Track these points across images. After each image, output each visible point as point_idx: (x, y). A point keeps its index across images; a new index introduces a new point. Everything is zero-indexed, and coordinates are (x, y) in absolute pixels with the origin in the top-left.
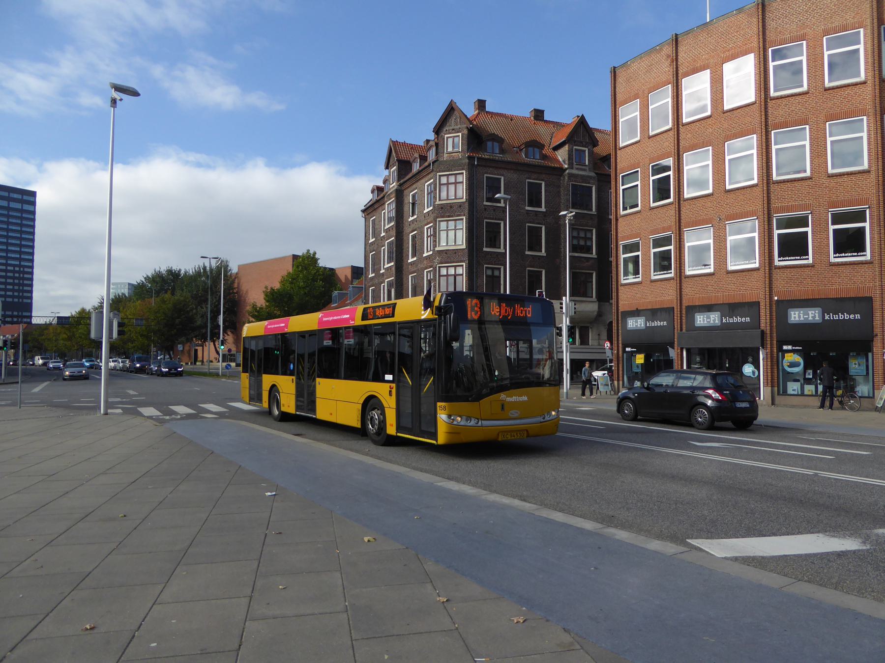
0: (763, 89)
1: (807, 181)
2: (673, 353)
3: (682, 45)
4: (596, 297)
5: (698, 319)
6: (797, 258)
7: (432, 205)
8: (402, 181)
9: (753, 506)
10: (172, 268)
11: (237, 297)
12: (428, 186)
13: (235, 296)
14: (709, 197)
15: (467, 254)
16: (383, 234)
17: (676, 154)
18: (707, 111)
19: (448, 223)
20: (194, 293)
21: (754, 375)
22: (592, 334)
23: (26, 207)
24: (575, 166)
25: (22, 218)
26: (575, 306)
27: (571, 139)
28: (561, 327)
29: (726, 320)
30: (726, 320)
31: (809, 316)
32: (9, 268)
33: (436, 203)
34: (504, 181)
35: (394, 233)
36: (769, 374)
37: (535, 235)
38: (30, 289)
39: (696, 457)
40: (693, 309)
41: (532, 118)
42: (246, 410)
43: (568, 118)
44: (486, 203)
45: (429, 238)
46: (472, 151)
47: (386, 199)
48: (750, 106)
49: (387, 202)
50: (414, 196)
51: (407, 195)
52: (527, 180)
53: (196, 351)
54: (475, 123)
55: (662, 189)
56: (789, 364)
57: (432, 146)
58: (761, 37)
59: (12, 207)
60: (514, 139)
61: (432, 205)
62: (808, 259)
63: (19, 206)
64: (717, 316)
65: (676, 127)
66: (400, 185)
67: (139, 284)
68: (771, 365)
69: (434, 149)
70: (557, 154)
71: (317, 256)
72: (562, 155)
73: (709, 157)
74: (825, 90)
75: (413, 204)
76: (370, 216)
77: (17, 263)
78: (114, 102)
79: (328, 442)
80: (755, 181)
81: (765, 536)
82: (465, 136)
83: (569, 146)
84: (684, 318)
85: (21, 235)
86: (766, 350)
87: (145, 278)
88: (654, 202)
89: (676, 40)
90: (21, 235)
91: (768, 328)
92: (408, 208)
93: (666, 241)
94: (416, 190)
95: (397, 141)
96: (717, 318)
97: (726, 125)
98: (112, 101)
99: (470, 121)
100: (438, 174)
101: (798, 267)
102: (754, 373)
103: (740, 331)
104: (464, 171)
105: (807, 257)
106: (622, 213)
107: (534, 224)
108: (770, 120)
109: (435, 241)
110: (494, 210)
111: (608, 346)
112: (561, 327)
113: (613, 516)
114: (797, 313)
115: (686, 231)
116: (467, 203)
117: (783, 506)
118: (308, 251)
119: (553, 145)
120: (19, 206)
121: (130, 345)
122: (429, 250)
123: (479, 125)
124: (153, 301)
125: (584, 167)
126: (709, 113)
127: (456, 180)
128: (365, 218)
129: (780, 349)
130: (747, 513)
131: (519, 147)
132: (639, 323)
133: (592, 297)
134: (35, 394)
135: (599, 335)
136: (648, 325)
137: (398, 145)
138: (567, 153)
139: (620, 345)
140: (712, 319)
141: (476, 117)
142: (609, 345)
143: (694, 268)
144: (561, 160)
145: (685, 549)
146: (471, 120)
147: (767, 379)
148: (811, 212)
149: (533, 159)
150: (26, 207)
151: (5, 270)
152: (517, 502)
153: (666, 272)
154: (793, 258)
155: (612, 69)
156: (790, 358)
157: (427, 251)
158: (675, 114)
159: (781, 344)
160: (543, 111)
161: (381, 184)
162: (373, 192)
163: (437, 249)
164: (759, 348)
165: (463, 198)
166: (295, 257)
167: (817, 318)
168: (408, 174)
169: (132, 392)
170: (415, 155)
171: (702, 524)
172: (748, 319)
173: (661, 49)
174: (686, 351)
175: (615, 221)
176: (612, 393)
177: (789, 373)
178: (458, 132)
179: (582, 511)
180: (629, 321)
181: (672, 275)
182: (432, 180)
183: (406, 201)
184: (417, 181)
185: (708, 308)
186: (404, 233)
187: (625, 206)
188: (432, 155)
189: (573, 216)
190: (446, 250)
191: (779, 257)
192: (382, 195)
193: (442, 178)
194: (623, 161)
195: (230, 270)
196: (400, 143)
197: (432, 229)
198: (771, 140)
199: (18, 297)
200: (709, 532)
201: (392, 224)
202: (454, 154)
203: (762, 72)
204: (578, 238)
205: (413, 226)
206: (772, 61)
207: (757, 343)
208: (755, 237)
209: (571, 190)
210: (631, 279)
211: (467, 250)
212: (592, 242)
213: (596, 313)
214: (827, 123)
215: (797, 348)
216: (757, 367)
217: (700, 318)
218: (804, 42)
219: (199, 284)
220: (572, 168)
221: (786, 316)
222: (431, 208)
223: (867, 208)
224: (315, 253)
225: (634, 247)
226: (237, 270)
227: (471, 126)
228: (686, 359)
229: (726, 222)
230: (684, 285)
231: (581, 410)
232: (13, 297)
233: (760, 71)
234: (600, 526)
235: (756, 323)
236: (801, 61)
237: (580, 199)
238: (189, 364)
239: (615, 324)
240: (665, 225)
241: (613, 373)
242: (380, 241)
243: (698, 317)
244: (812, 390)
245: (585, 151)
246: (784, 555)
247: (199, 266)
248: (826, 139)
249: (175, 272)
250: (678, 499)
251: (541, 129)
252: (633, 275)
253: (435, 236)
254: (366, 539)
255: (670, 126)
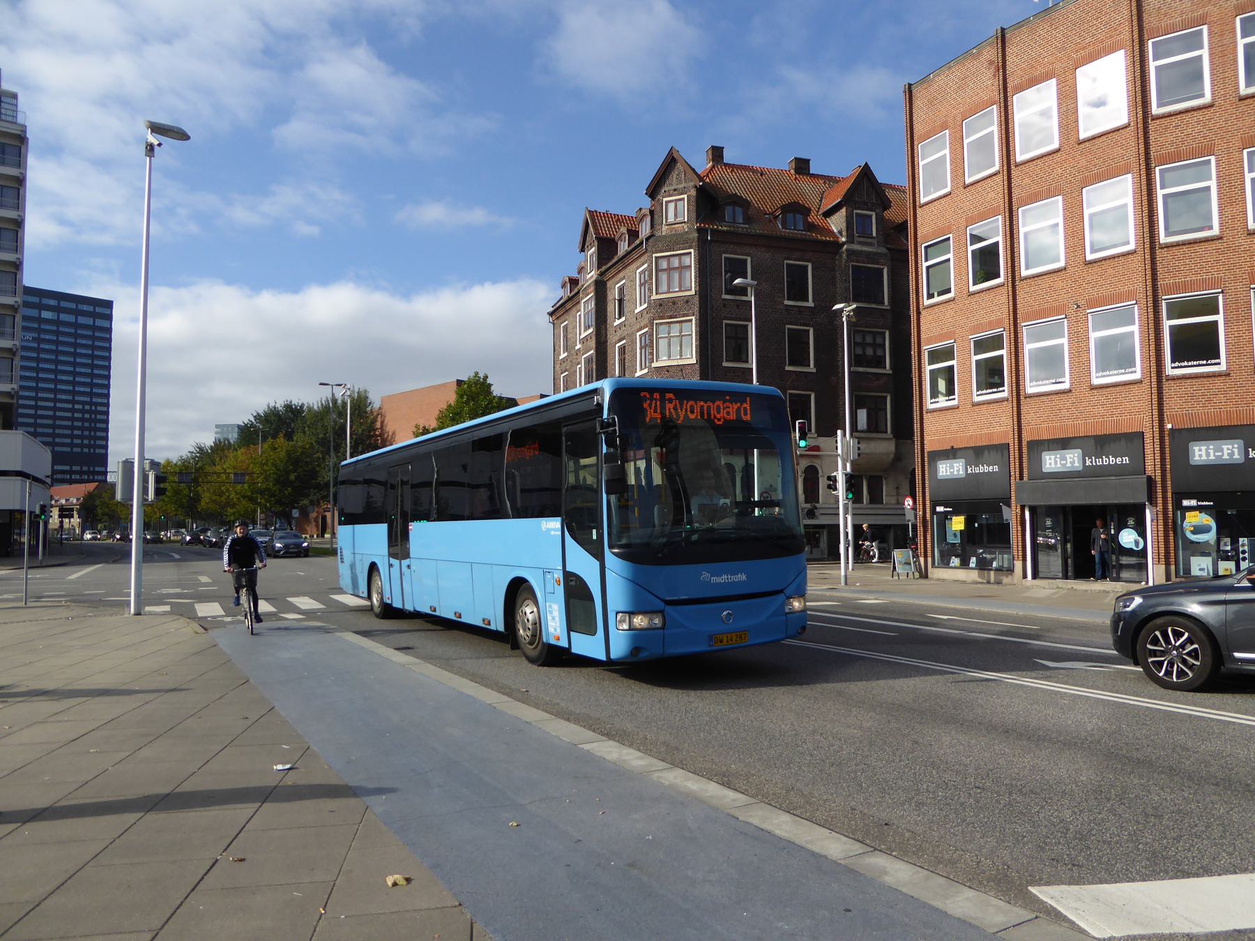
0: (1139, 103)
1: (1214, 242)
2: (1010, 514)
3: (1012, 44)
4: (892, 432)
5: (1048, 460)
6: (1201, 362)
7: (647, 301)
8: (604, 268)
9: (1157, 798)
10: (291, 402)
11: (379, 441)
12: (640, 274)
13: (378, 440)
14: (1060, 273)
15: (698, 372)
16: (578, 346)
17: (1007, 210)
18: (1052, 143)
19: (670, 326)
20: (320, 436)
21: (1137, 546)
22: (887, 487)
23: (99, 323)
24: (857, 239)
25: (93, 338)
26: (859, 446)
27: (849, 200)
28: (835, 476)
29: (1091, 462)
30: (1091, 462)
31: (1223, 453)
32: (77, 406)
33: (652, 298)
34: (752, 264)
35: (593, 343)
36: (1162, 546)
37: (799, 341)
38: (104, 434)
39: (1047, 690)
40: (1038, 446)
41: (792, 171)
42: (352, 607)
43: (846, 170)
44: (725, 296)
45: (643, 350)
46: (703, 221)
47: (581, 295)
48: (1121, 131)
49: (582, 299)
50: (621, 289)
51: (610, 289)
52: (786, 262)
53: (324, 518)
54: (708, 180)
55: (986, 263)
56: (1192, 529)
57: (645, 215)
58: (1135, 23)
59: (35, 310)
60: (767, 201)
61: (647, 301)
62: (1219, 364)
63: (89, 321)
64: (961, 464)
65: (1005, 168)
66: (602, 274)
67: (246, 425)
68: (1164, 531)
69: (649, 219)
70: (830, 222)
71: (489, 381)
72: (837, 223)
73: (1058, 207)
74: (1240, 100)
75: (621, 301)
76: (560, 321)
77: (88, 399)
78: (150, 149)
79: (445, 663)
80: (1132, 246)
81: (1187, 875)
82: (693, 199)
83: (846, 209)
84: (1025, 460)
85: (38, 354)
86: (1157, 507)
87: (255, 417)
88: (974, 284)
89: (1003, 38)
90: (38, 354)
91: (1158, 473)
92: (612, 308)
93: (996, 342)
94: (624, 281)
95: (596, 212)
96: (1076, 459)
97: (1083, 162)
98: (146, 148)
99: (700, 178)
100: (654, 255)
101: (1203, 377)
102: (1137, 543)
103: (1113, 478)
104: (692, 251)
105: (1217, 361)
106: (927, 302)
107: (797, 325)
108: (1153, 150)
109: (652, 354)
110: (738, 306)
111: (909, 505)
112: (835, 476)
113: (886, 824)
114: (1204, 448)
115: (1025, 326)
116: (697, 296)
117: (1215, 798)
118: (477, 373)
119: (824, 209)
120: (89, 321)
121: (230, 511)
122: (643, 366)
123: (713, 183)
124: (261, 449)
125: (870, 240)
126: (1056, 145)
127: (680, 263)
128: (554, 324)
129: (1178, 506)
130: (1147, 815)
131: (774, 212)
132: (956, 469)
133: (886, 432)
134: (72, 582)
135: (897, 488)
136: (969, 471)
137: (597, 217)
138: (844, 219)
139: (928, 503)
140: (1069, 460)
141: (710, 172)
142: (911, 503)
143: (1038, 383)
144: (835, 231)
145: (1025, 914)
146: (702, 176)
147: (1159, 553)
148: (1222, 291)
149: (795, 229)
150: (99, 323)
151: (53, 407)
152: (712, 790)
153: (995, 390)
154: (1195, 363)
155: (907, 87)
156: (1193, 519)
157: (641, 369)
158: (1004, 149)
159: (1179, 496)
160: (808, 161)
161: (575, 275)
162: (563, 286)
163: (654, 365)
164: (1145, 504)
165: (691, 290)
166: (459, 383)
167: (1236, 456)
168: (612, 258)
169: (204, 579)
170: (621, 230)
171: (1059, 843)
172: (1126, 460)
173: (980, 53)
174: (1029, 511)
175: (915, 315)
176: (917, 575)
177: (1192, 542)
178: (682, 194)
179: (831, 810)
180: (941, 466)
181: (1005, 395)
182: (646, 266)
183: (610, 297)
184: (626, 267)
185: (1063, 444)
186: (608, 343)
187: (931, 293)
188: (645, 230)
189: (853, 310)
190: (668, 366)
191: (1173, 361)
192: (576, 290)
193: (660, 261)
194: (926, 226)
195: (370, 403)
196: (600, 213)
197: (647, 336)
198: (1155, 181)
199: (89, 446)
200: (1074, 865)
201: (591, 330)
202: (676, 226)
203: (1138, 78)
204: (863, 345)
205: (619, 333)
206: (1154, 60)
207: (1142, 497)
208: (1133, 332)
209: (851, 275)
210: (942, 402)
211: (697, 366)
212: (885, 350)
213: (892, 456)
214: (1245, 152)
215: (1205, 503)
216: (1142, 534)
217: (1050, 459)
218: (1205, 28)
219: (326, 424)
220: (853, 242)
221: (1186, 453)
222: (646, 306)
223: (1219, 293)
224: (486, 377)
225: (948, 353)
226: (380, 403)
227: (701, 184)
228: (1030, 523)
229: (1088, 311)
230: (1024, 409)
231: (865, 603)
232: (82, 446)
233: (1135, 77)
234: (857, 848)
235: (1138, 466)
236: (1200, 58)
237: (864, 287)
238: (315, 536)
239: (918, 472)
240: (993, 318)
241: (917, 546)
242: (574, 355)
243: (1047, 457)
244: (1231, 570)
245: (870, 217)
246: (1235, 930)
247: (327, 399)
248: (1244, 175)
249: (296, 407)
250: (1014, 782)
251: (806, 186)
252: (946, 396)
253: (649, 344)
254: (390, 881)
255: (997, 168)
